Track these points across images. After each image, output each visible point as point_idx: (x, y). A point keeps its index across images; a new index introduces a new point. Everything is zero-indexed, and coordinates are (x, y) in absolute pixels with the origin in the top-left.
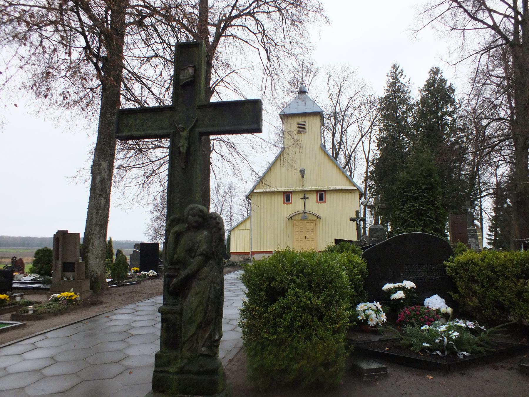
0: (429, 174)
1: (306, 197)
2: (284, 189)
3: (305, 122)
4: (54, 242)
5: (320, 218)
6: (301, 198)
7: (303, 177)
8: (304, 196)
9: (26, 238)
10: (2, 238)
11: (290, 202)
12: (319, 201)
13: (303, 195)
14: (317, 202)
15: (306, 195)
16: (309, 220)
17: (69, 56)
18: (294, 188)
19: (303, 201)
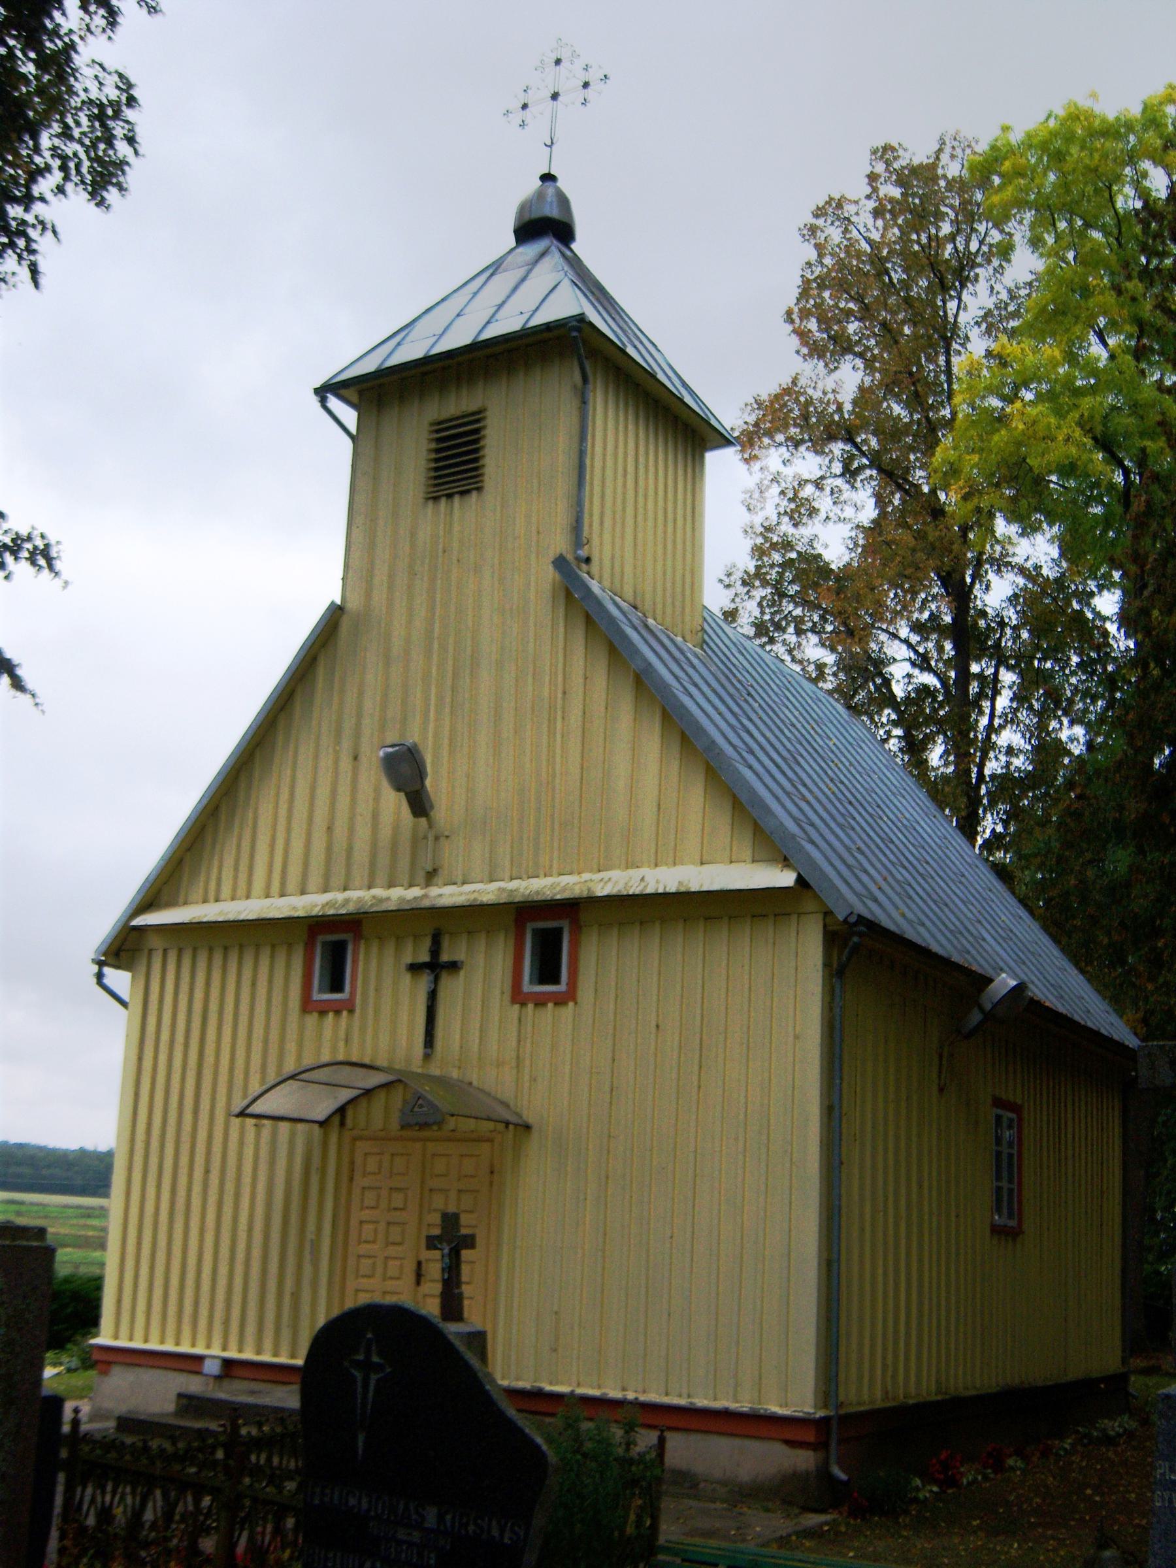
0: (952, 464)
1: (445, 957)
2: (340, 896)
3: (478, 416)
4: (821, 1172)
5: (528, 1127)
6: (414, 968)
7: (419, 804)
8: (435, 951)
9: (20, 1146)
10: (5, 1145)
11: (317, 996)
12: (527, 987)
13: (427, 943)
14: (518, 997)
15: (446, 943)
16: (454, 1138)
17: (999, 571)
18: (354, 894)
19: (424, 982)
